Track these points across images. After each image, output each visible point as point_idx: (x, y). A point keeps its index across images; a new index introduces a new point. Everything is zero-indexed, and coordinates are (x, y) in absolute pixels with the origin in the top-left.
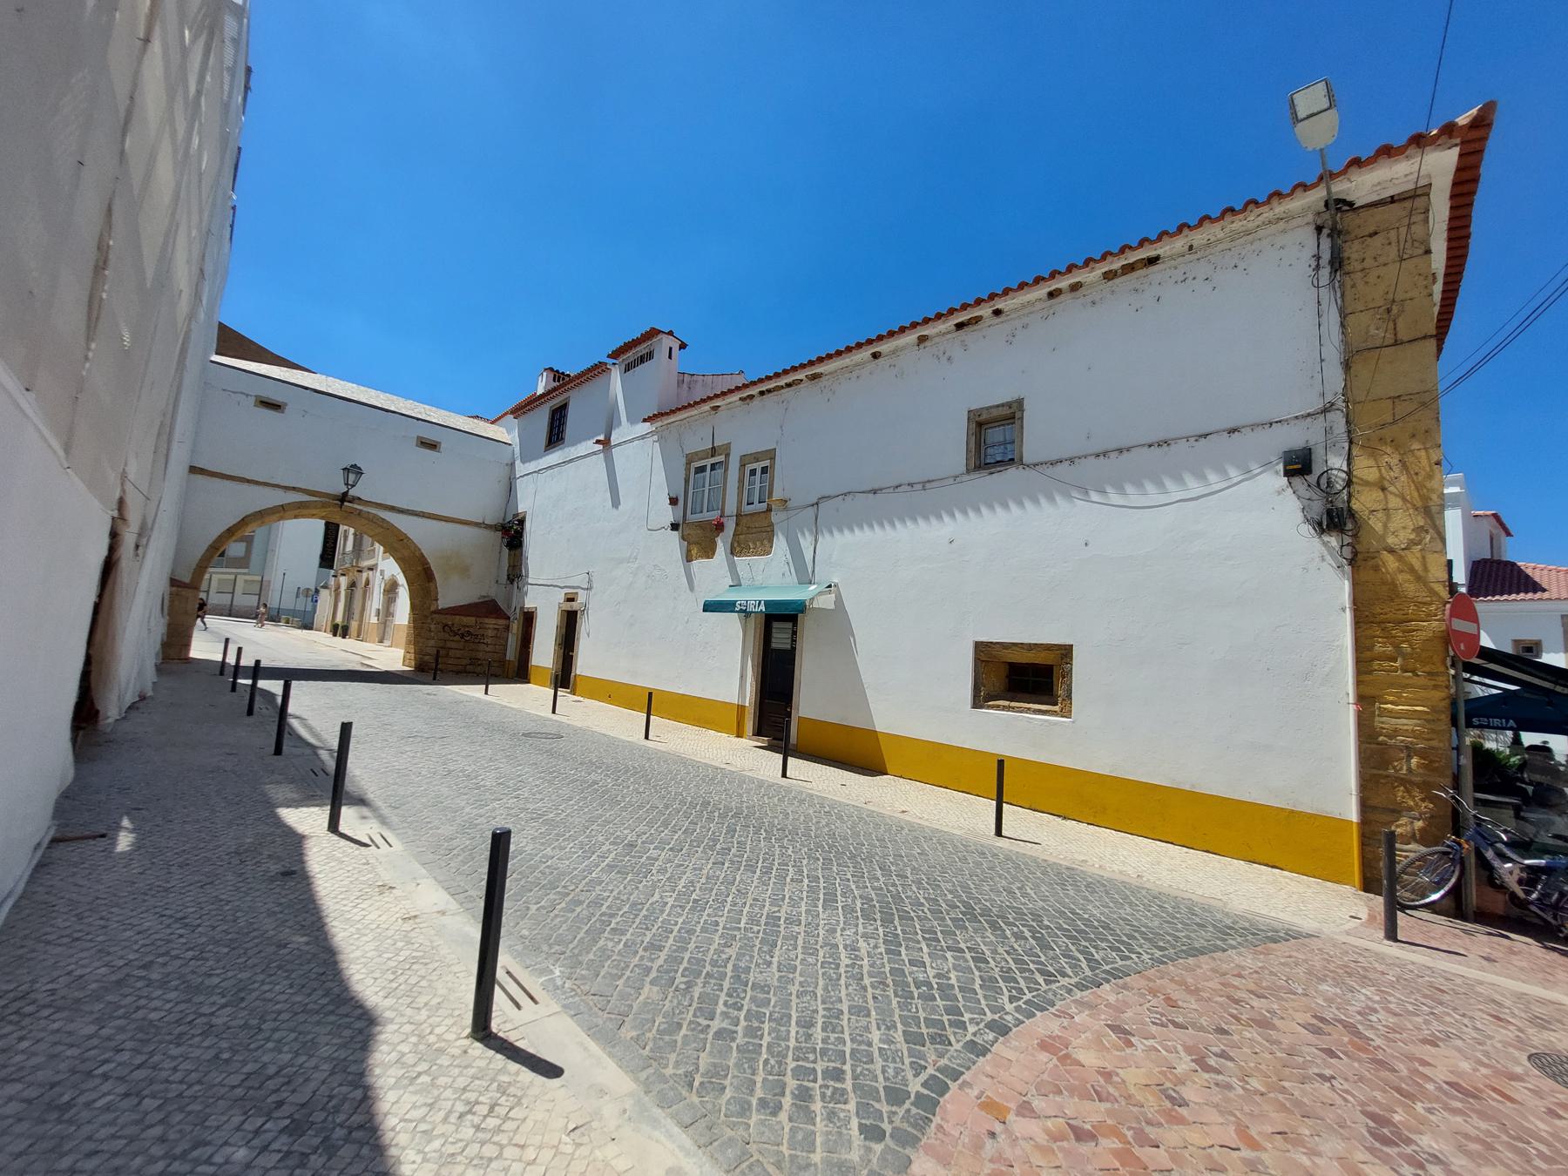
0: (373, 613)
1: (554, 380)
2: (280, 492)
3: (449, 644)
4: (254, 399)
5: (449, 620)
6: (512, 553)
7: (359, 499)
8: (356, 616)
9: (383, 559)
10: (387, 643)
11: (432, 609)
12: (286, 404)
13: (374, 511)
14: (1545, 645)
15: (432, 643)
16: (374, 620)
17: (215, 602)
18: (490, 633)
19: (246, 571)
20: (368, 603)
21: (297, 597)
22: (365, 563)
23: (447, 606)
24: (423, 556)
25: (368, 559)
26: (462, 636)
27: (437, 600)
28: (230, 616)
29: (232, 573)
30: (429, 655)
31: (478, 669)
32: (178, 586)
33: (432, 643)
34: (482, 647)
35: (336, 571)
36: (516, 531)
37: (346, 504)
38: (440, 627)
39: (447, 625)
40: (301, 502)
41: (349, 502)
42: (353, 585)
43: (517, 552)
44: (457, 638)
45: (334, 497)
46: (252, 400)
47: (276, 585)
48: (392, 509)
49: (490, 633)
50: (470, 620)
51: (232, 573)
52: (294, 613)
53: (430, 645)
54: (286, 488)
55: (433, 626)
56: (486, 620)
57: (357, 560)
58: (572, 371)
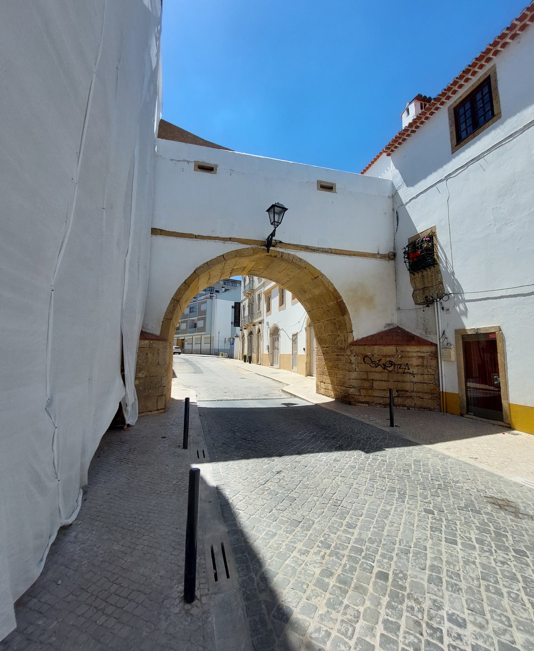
0: (265, 348)
1: (422, 108)
2: (220, 243)
3: (371, 377)
4: (193, 164)
5: (368, 350)
6: (418, 275)
7: (281, 242)
8: (255, 350)
9: (267, 316)
10: (276, 366)
11: (350, 341)
12: (217, 166)
13: (292, 252)
14: (459, 327)
15: (354, 375)
16: (266, 352)
17: (195, 348)
18: (415, 362)
19: (204, 333)
20: (261, 343)
21: (225, 343)
22: (256, 321)
23: (360, 337)
24: (335, 290)
25: (257, 318)
26: (385, 367)
27: (352, 332)
28: (200, 354)
29: (190, 336)
30: (353, 387)
31: (408, 402)
32: (150, 339)
33: (354, 375)
34: (408, 377)
35: (241, 327)
36: (427, 249)
37: (271, 248)
38: (360, 358)
39: (366, 356)
40: (237, 251)
41: (274, 246)
42: (251, 333)
43: (428, 273)
44: (379, 369)
45: (262, 243)
46: (192, 165)
47: (216, 339)
48: (307, 248)
49: (415, 362)
50: (390, 350)
51: (190, 336)
52: (224, 351)
53: (353, 377)
54: (224, 240)
55: (353, 359)
56: (408, 349)
57: (252, 320)
58: (433, 95)
